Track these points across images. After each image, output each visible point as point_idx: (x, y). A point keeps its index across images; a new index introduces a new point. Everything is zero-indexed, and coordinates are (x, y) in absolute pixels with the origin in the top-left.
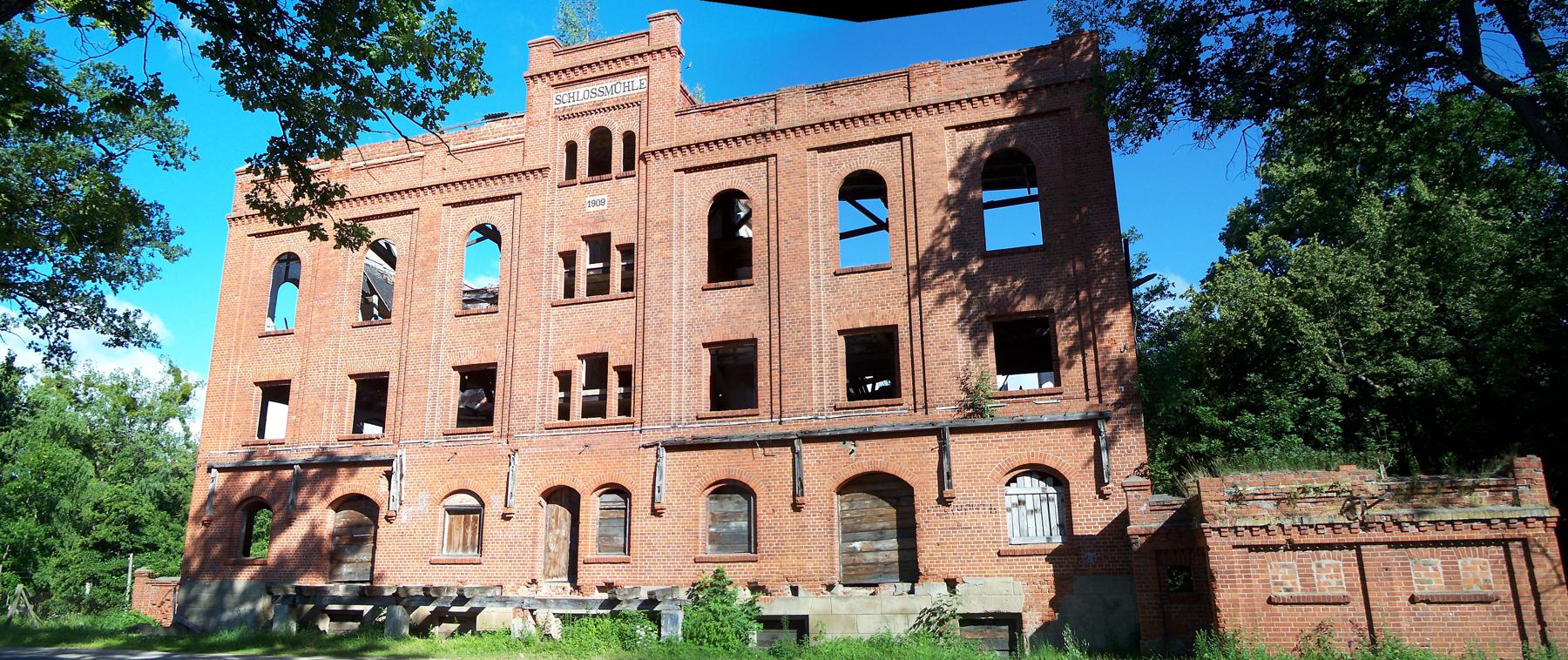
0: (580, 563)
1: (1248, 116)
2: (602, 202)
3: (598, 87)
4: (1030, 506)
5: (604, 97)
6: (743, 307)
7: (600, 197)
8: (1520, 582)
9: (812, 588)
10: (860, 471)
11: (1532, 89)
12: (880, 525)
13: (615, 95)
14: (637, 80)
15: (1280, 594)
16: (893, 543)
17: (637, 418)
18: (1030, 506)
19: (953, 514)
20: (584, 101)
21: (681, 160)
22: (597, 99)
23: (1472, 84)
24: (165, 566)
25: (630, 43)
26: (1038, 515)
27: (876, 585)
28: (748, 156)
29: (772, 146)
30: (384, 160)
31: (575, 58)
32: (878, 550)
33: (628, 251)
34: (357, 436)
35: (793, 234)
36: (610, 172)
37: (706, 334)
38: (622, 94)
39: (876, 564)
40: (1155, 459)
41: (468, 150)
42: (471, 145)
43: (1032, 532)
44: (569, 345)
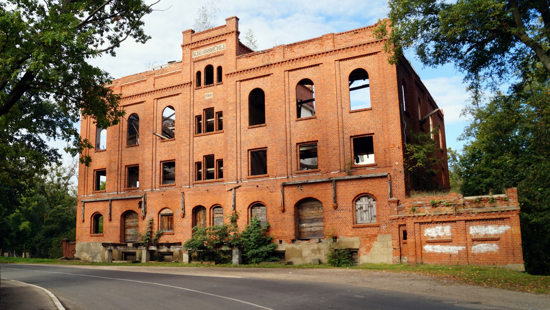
0: (371, 224)
1: (51, 68)
3: (208, 48)
4: (364, 209)
6: (262, 135)
8: (520, 244)
9: (287, 241)
10: (304, 197)
11: (535, 16)
12: (312, 217)
13: (214, 51)
14: (222, 45)
15: (429, 239)
16: (128, 233)
17: (250, 176)
18: (364, 209)
19: (337, 213)
20: (203, 54)
23: (85, 162)
24: (439, 280)
25: (220, 30)
26: (367, 212)
27: (309, 240)
28: (263, 75)
29: (271, 70)
30: (133, 82)
31: (129, 205)
32: (311, 227)
33: (220, 114)
34: (299, 119)
35: (280, 105)
36: (265, 123)
37: (249, 146)
38: (217, 51)
39: (311, 232)
40: (130, 120)
41: (162, 76)
42: (163, 74)
43: (365, 219)
44: (200, 152)
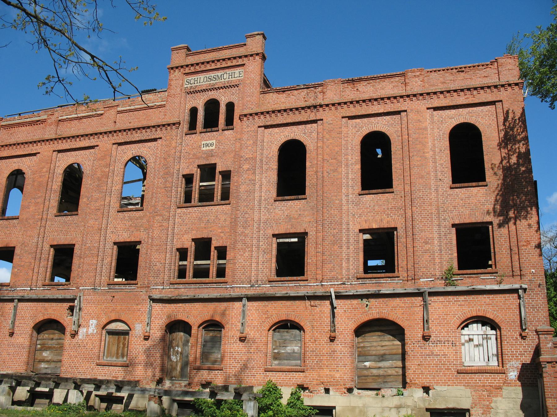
2: (212, 145)
3: (213, 75)
5: (216, 81)
7: (211, 142)
13: (223, 80)
21: (262, 120)
22: (212, 82)
29: (320, 114)
32: (380, 368)
38: (227, 80)
42: (132, 107)
43: (477, 359)
